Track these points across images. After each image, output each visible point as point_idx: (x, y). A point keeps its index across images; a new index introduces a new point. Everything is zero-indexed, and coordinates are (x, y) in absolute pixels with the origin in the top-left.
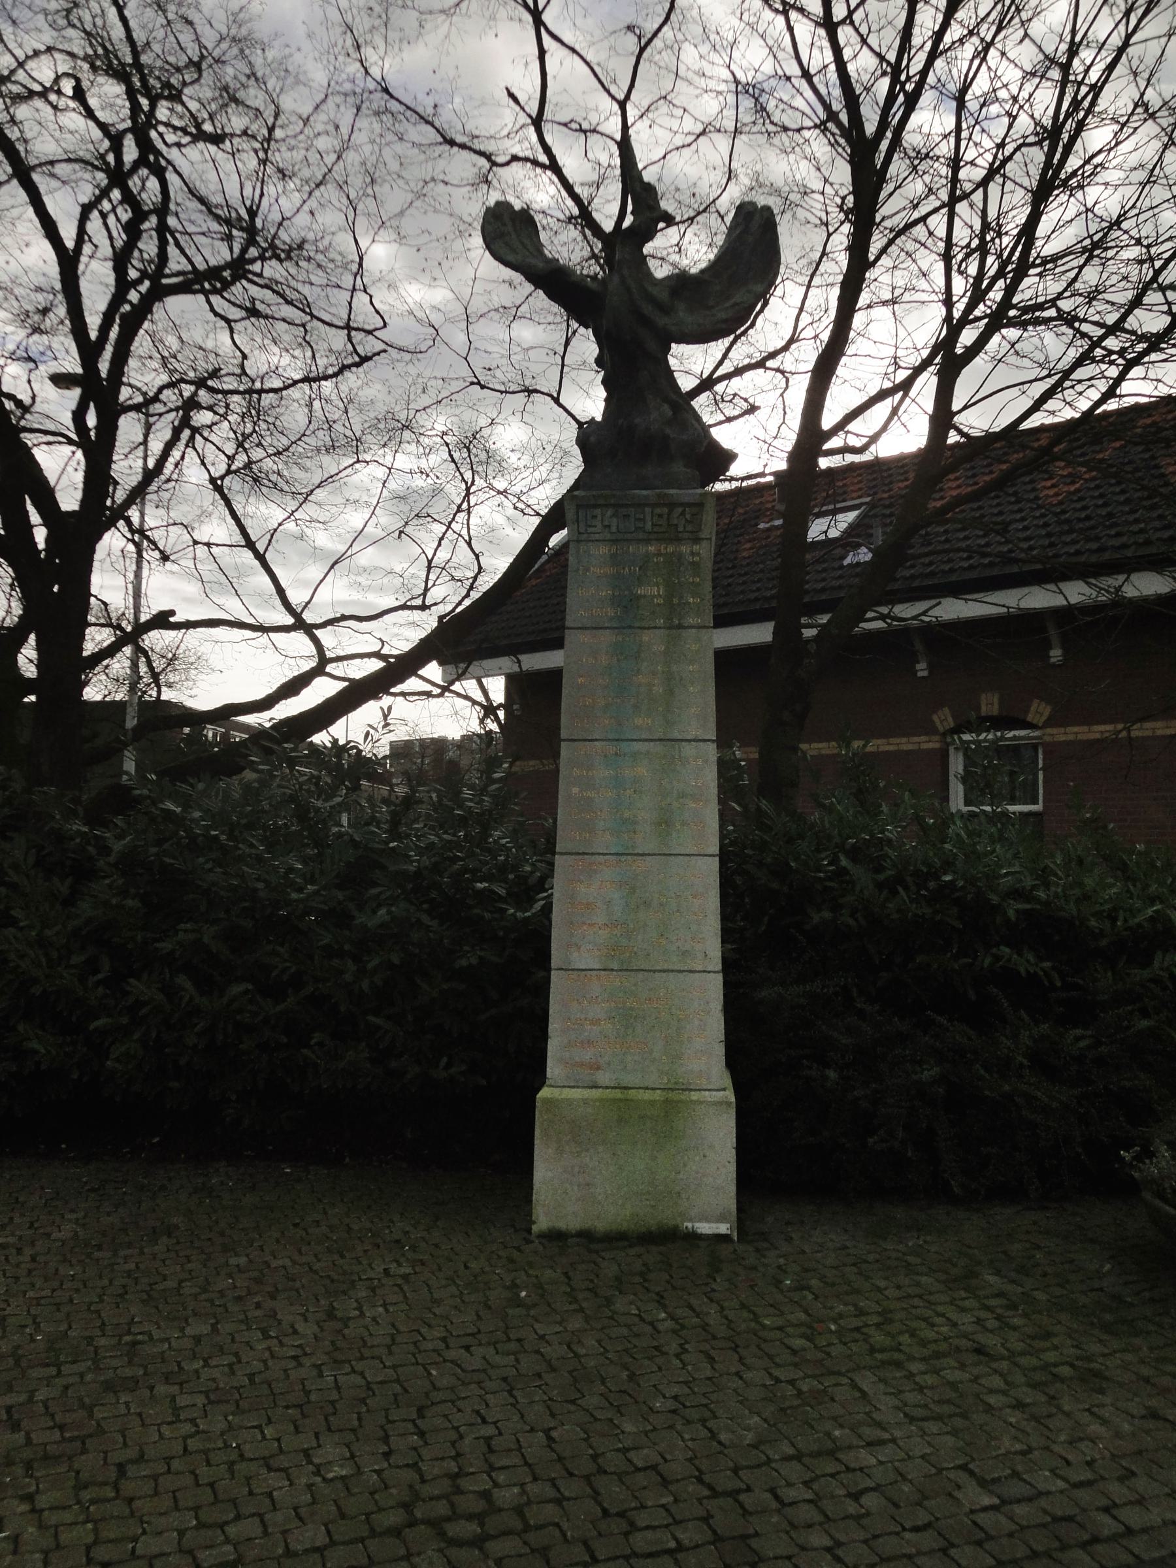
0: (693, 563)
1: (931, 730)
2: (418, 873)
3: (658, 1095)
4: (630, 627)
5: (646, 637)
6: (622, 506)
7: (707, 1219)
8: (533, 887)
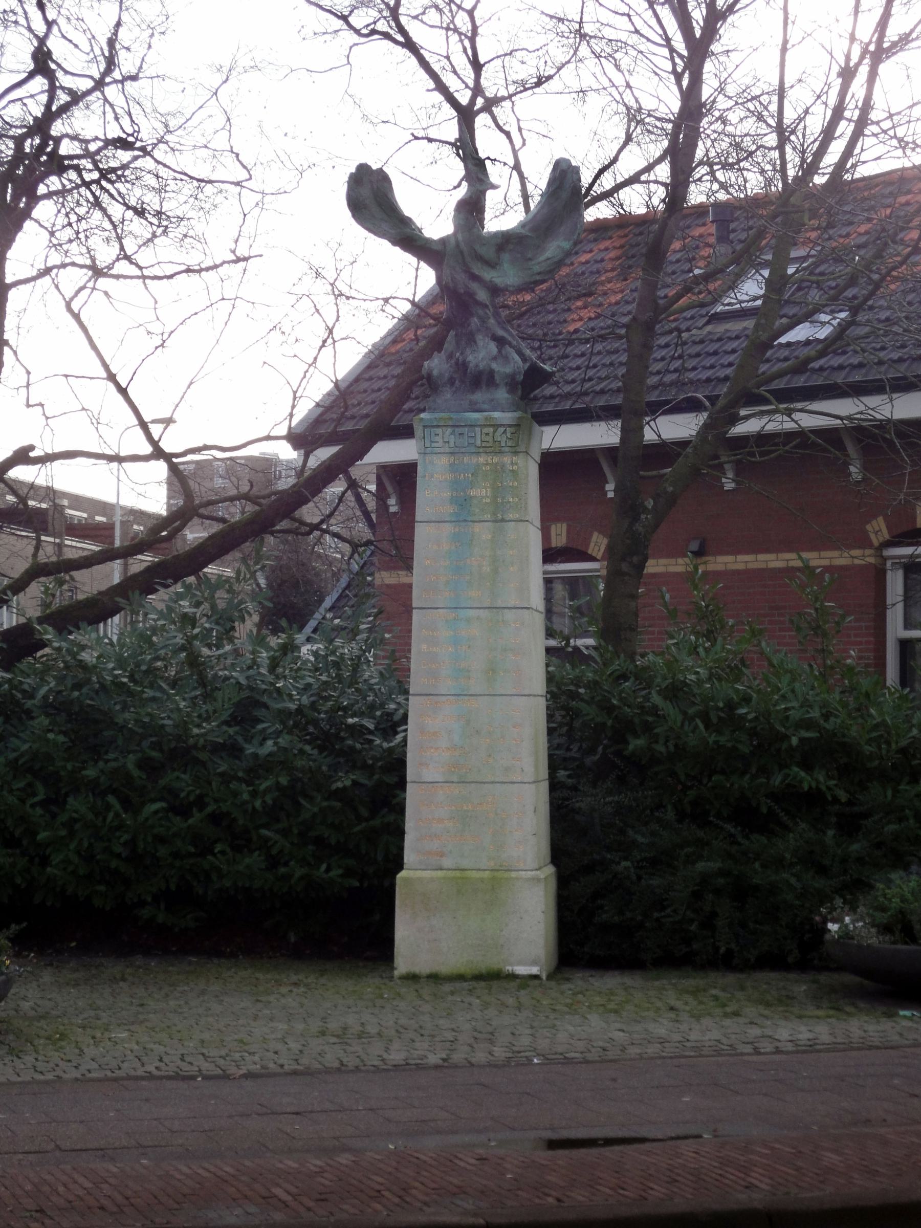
0: (513, 471)
1: (863, 542)
2: (299, 710)
3: (487, 874)
4: (465, 521)
5: (477, 528)
6: (458, 426)
7: (520, 963)
8: (394, 724)
